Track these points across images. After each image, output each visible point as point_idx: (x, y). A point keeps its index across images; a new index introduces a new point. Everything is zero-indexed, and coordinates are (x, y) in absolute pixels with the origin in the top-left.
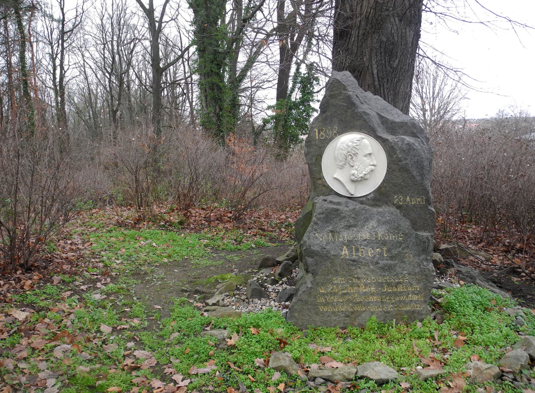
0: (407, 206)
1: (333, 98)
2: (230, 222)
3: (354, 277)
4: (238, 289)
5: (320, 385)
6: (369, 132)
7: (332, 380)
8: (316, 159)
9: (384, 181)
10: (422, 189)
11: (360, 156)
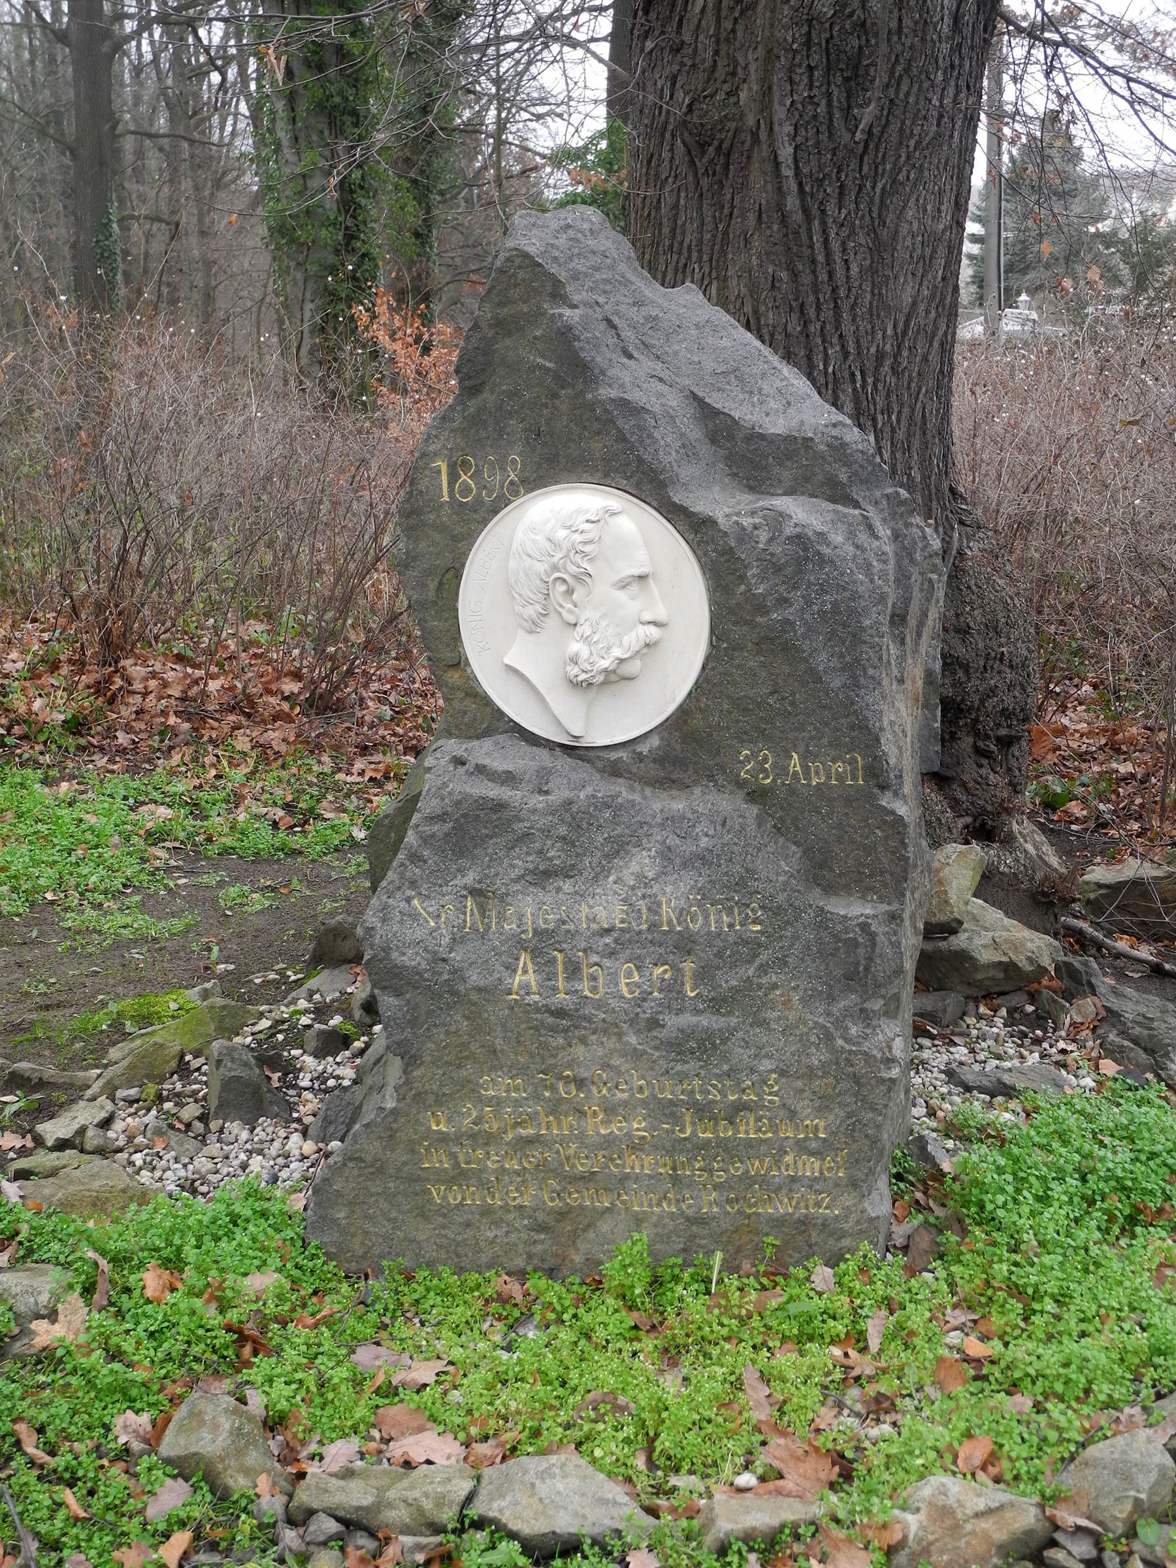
0: (792, 791)
1: (510, 334)
2: (288, 719)
3: (560, 1077)
4: (183, 1071)
5: (324, 1544)
6: (638, 485)
7: (374, 1524)
8: (440, 583)
9: (697, 685)
10: (852, 727)
11: (603, 588)
